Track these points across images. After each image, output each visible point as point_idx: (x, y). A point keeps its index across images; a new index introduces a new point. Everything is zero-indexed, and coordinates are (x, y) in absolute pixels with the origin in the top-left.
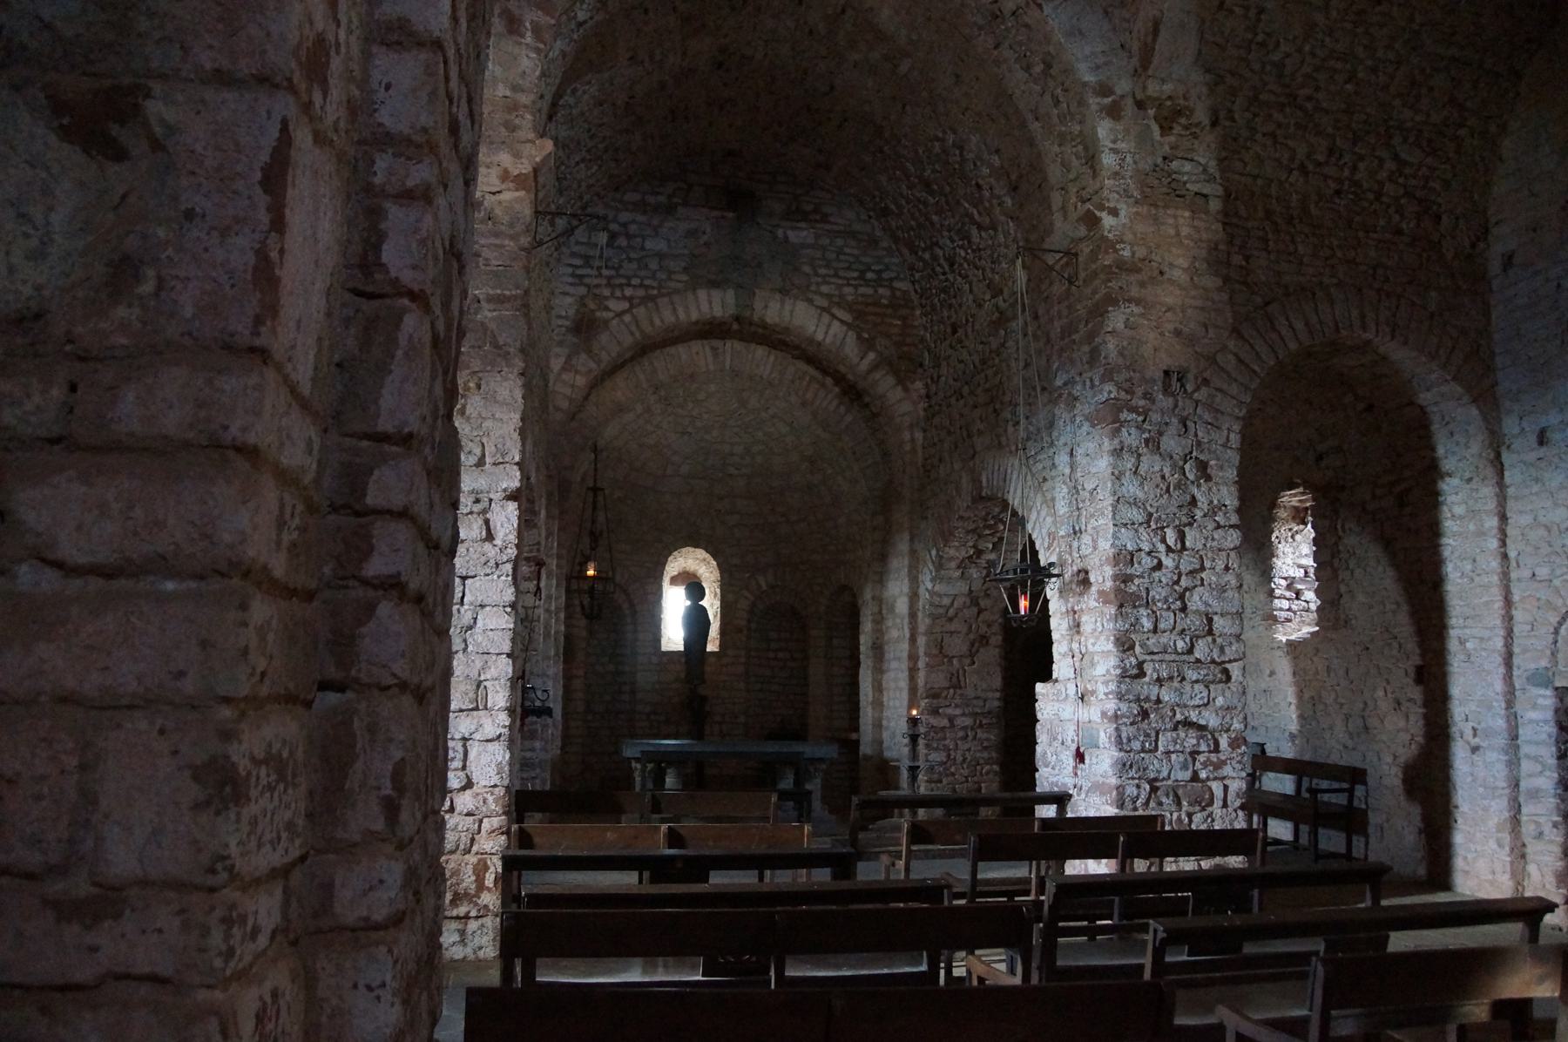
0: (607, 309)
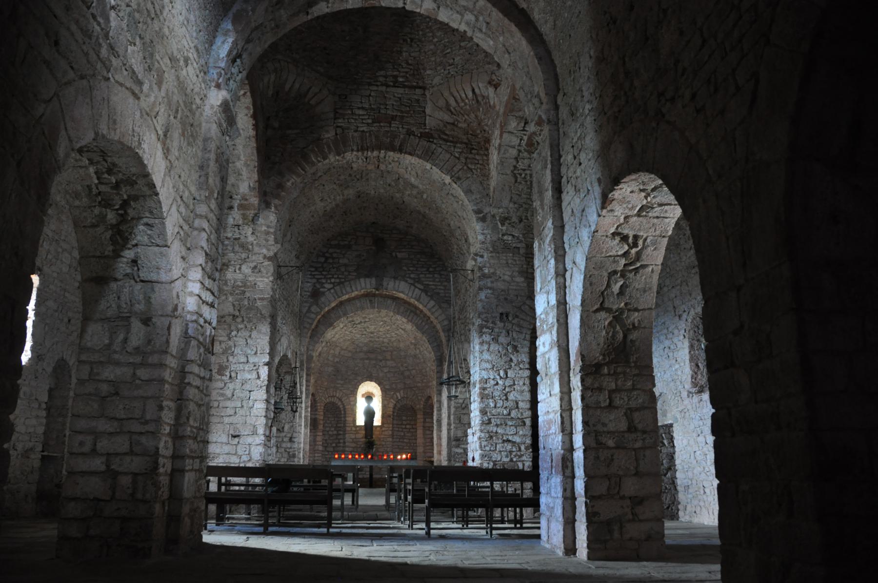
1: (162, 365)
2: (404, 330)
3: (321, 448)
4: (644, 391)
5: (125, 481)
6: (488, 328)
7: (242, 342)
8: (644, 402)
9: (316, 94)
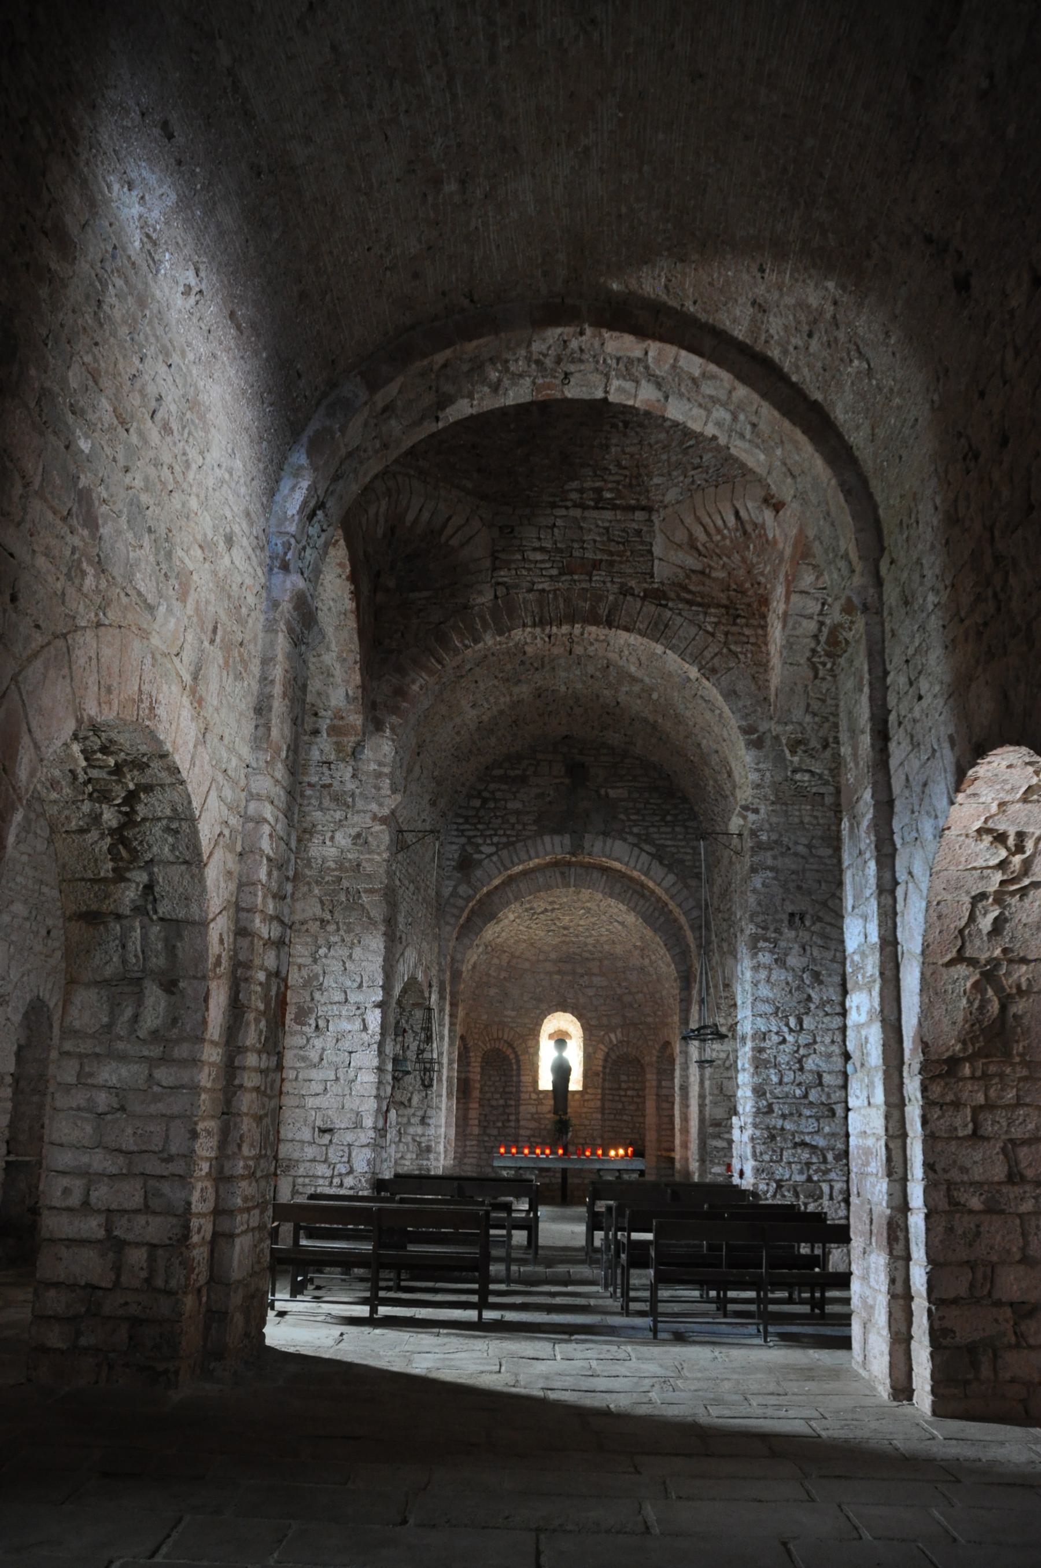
0: (481, 852)
1: (195, 1062)
2: (622, 924)
3: (476, 1130)
5: (137, 1257)
6: (766, 940)
7: (335, 966)
9: (459, 528)
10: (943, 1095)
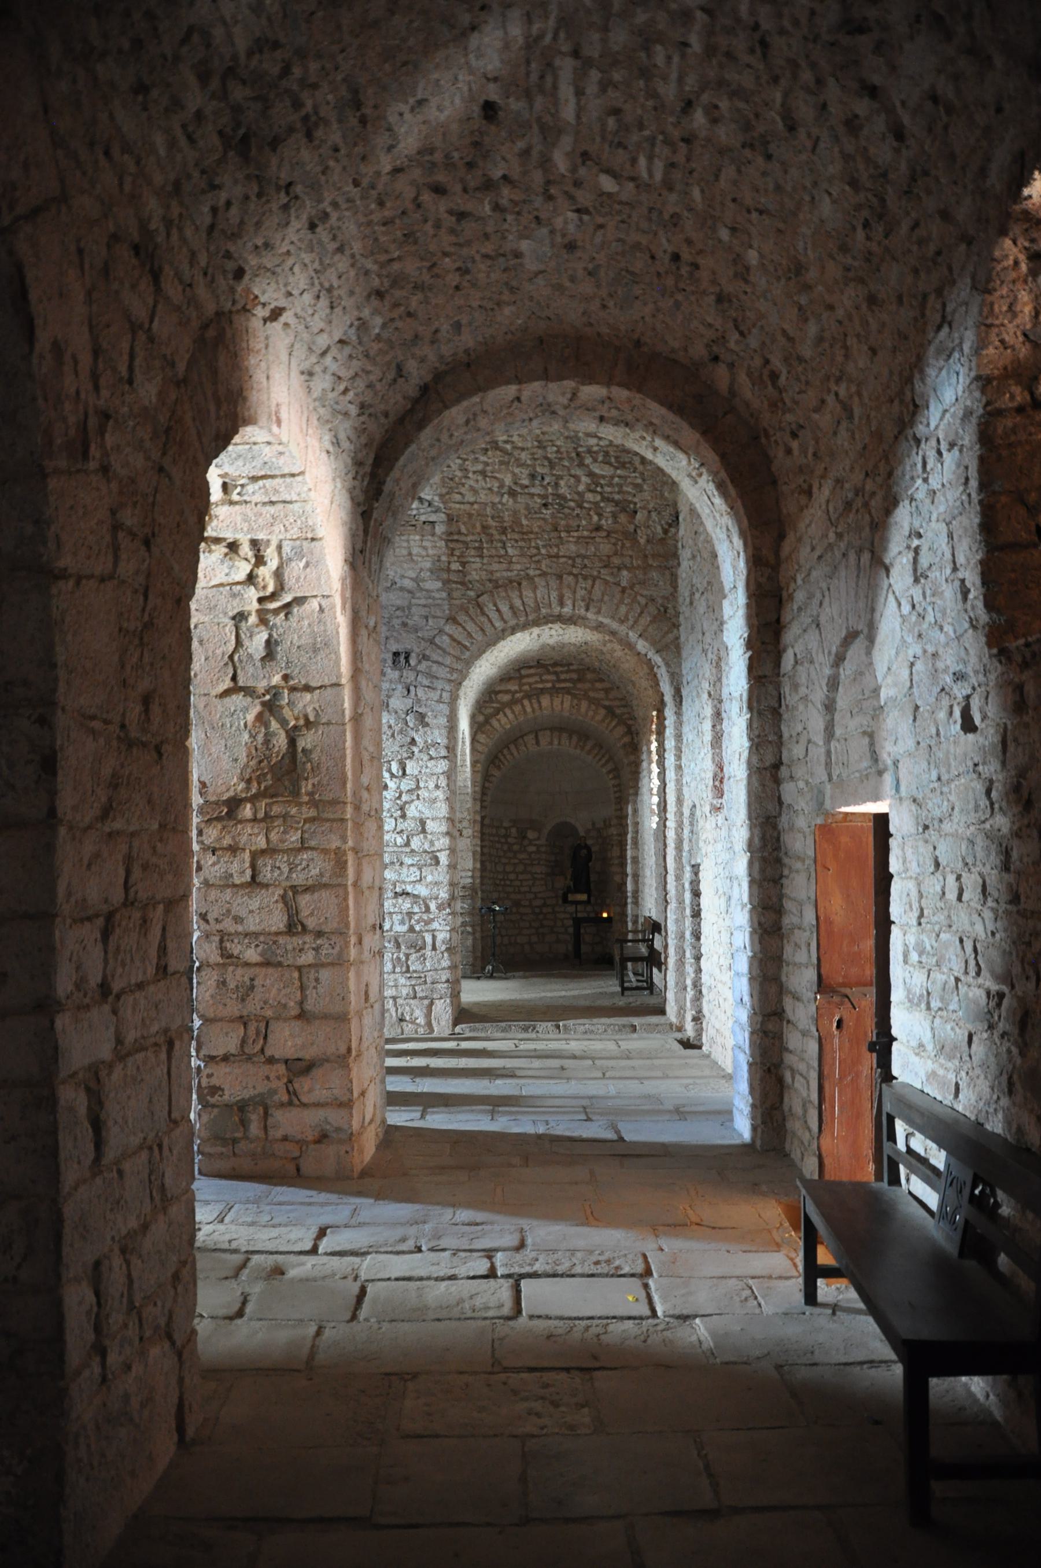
4: (325, 851)
8: (321, 875)
10: (219, 839)
